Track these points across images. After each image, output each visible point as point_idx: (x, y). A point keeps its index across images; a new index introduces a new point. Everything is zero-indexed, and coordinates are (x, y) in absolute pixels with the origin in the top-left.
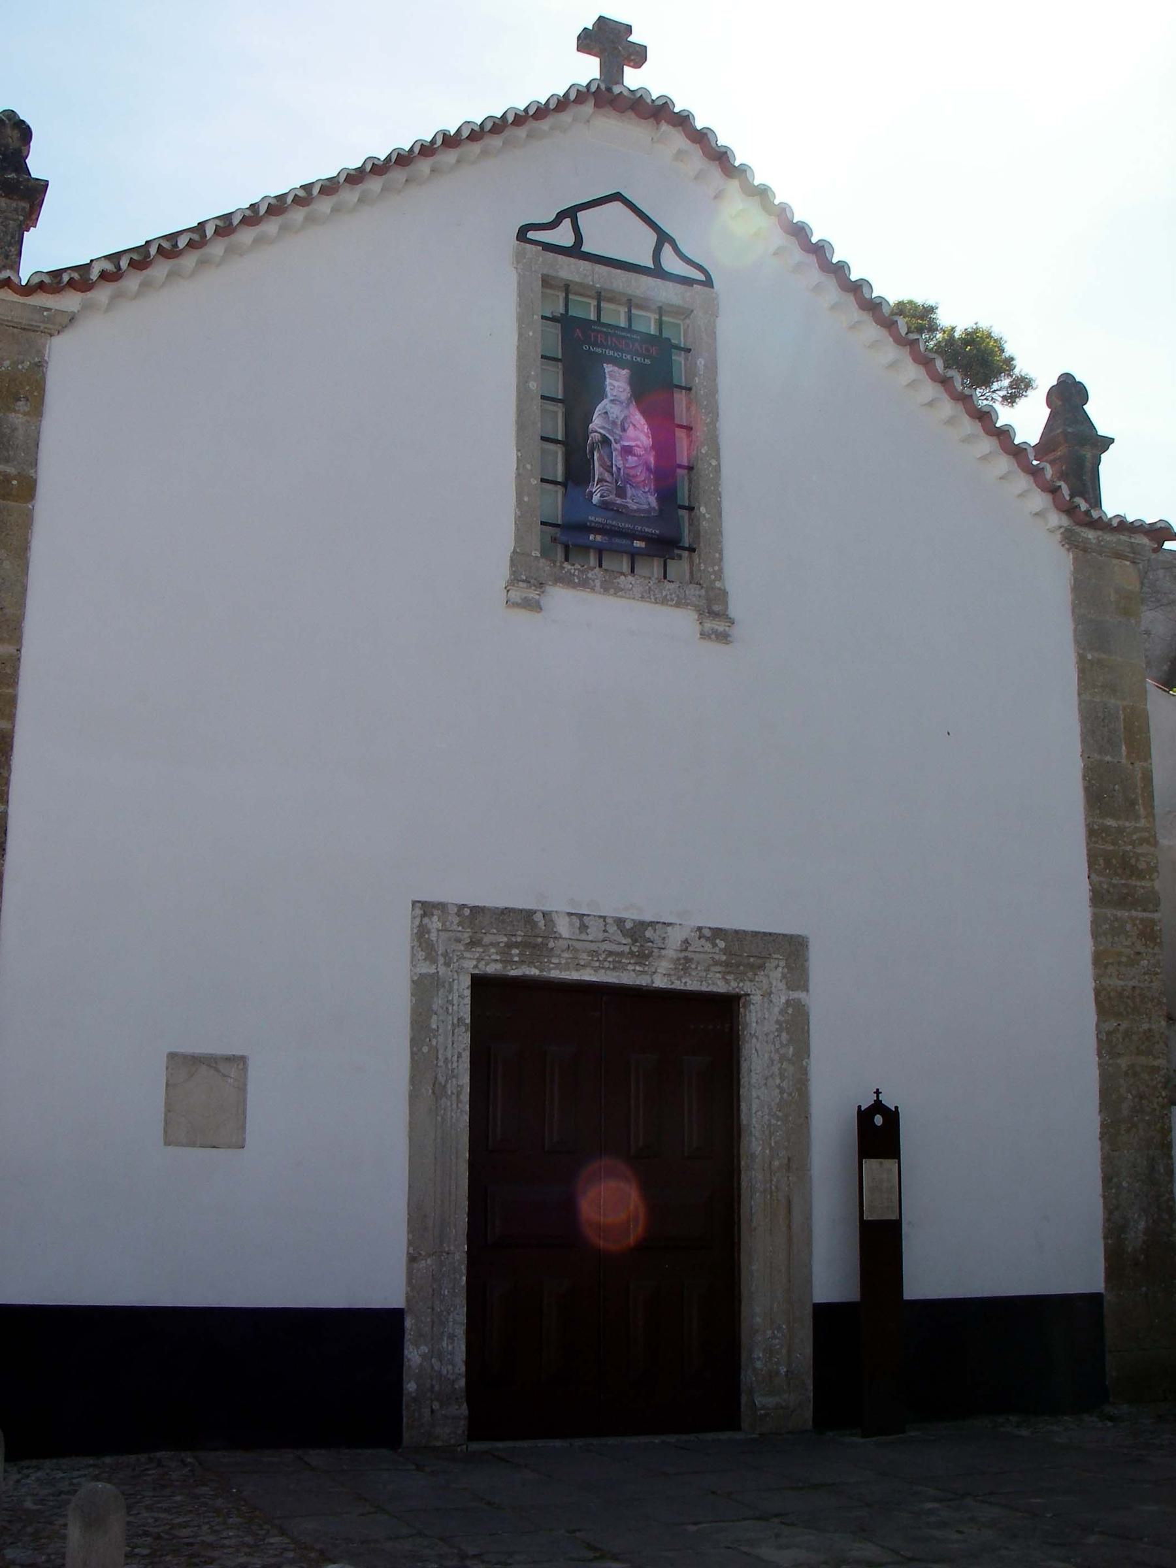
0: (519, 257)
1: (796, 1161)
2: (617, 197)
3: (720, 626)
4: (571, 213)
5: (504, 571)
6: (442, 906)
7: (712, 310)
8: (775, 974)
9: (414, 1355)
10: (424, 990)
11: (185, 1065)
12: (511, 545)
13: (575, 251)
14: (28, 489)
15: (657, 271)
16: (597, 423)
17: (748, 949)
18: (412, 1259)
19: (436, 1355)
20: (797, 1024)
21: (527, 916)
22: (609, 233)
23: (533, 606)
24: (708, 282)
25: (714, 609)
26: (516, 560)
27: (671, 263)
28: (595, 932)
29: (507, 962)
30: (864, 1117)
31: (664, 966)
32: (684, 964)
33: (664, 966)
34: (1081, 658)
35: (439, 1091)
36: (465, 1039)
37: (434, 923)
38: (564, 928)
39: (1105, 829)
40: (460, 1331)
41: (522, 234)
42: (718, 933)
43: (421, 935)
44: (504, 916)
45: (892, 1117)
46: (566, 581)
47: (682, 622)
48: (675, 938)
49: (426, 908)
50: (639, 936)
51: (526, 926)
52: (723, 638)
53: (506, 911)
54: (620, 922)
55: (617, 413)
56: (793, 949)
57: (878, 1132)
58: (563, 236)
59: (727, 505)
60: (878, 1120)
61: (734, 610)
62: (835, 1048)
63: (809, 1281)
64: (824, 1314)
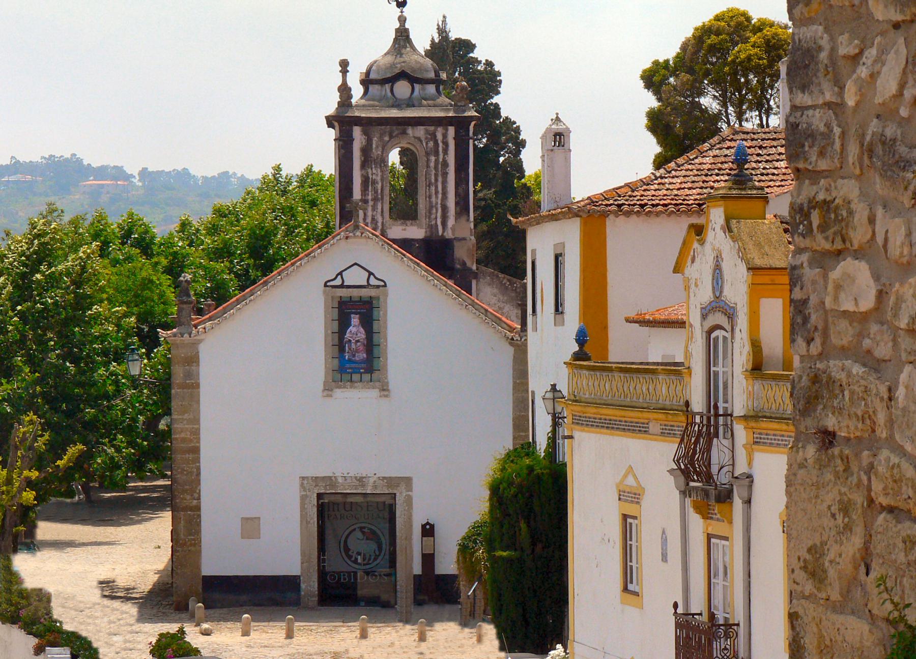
0: (324, 292)
1: (409, 538)
2: (356, 264)
3: (386, 393)
4: (340, 273)
5: (322, 387)
6: (307, 478)
7: (386, 295)
8: (402, 487)
9: (303, 586)
10: (303, 498)
11: (245, 520)
12: (323, 379)
13: (342, 286)
14: (198, 386)
15: (369, 285)
16: (347, 335)
17: (391, 481)
18: (302, 563)
19: (310, 586)
20: (409, 501)
21: (330, 478)
22: (355, 277)
23: (328, 396)
24: (385, 286)
25: (384, 389)
26: (325, 383)
27: (373, 281)
28: (349, 480)
29: (326, 489)
30: (423, 526)
31: (370, 488)
32: (375, 487)
33: (370, 488)
34: (514, 383)
35: (308, 523)
36: (315, 509)
37: (305, 482)
38: (340, 480)
39: (519, 436)
40: (316, 580)
41: (326, 285)
42: (384, 478)
43: (302, 485)
44: (324, 478)
45: (432, 526)
46: (340, 387)
47: (375, 393)
48: (372, 480)
49: (303, 478)
50: (361, 480)
51: (330, 480)
52: (386, 396)
53: (324, 477)
54: (356, 478)
55: (355, 330)
56: (408, 481)
57: (428, 530)
58: (338, 282)
59: (389, 356)
60: (428, 527)
61: (391, 387)
62: (420, 508)
63: (412, 568)
64: (415, 576)
